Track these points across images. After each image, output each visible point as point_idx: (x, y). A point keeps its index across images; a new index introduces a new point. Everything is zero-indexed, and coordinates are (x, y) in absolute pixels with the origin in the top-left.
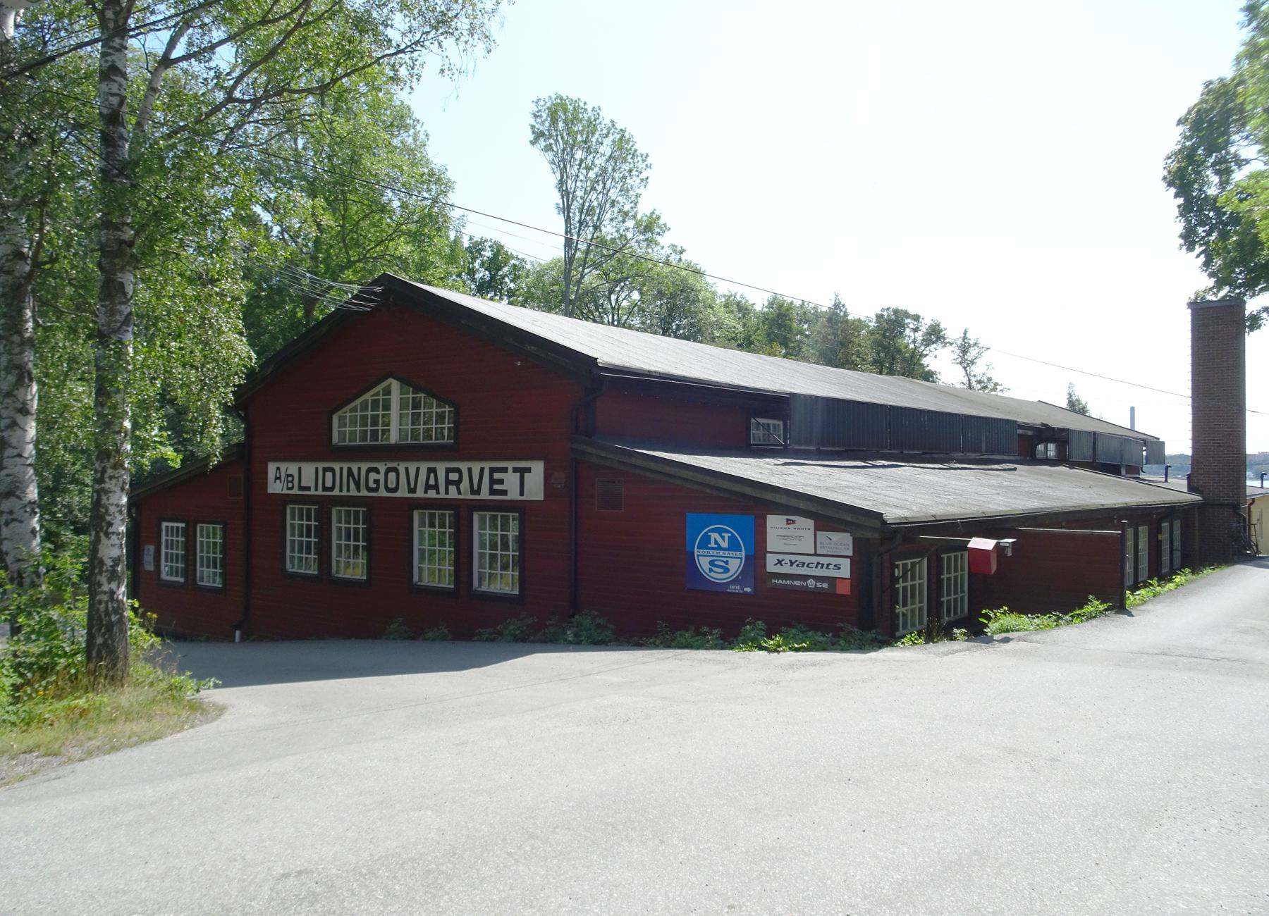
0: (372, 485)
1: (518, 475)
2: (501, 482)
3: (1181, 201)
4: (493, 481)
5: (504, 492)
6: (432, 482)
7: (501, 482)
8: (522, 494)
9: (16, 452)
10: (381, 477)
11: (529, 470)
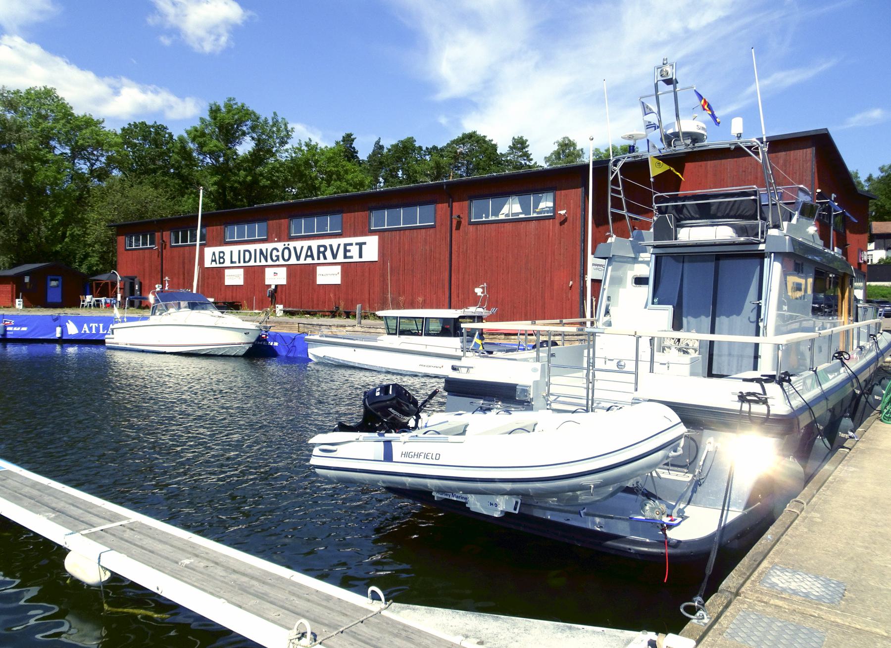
0: (275, 258)
1: (358, 247)
2: (349, 251)
3: (183, 304)
4: (346, 251)
5: (351, 257)
6: (309, 254)
7: (349, 251)
8: (361, 256)
9: (118, 85)
10: (280, 254)
11: (365, 243)
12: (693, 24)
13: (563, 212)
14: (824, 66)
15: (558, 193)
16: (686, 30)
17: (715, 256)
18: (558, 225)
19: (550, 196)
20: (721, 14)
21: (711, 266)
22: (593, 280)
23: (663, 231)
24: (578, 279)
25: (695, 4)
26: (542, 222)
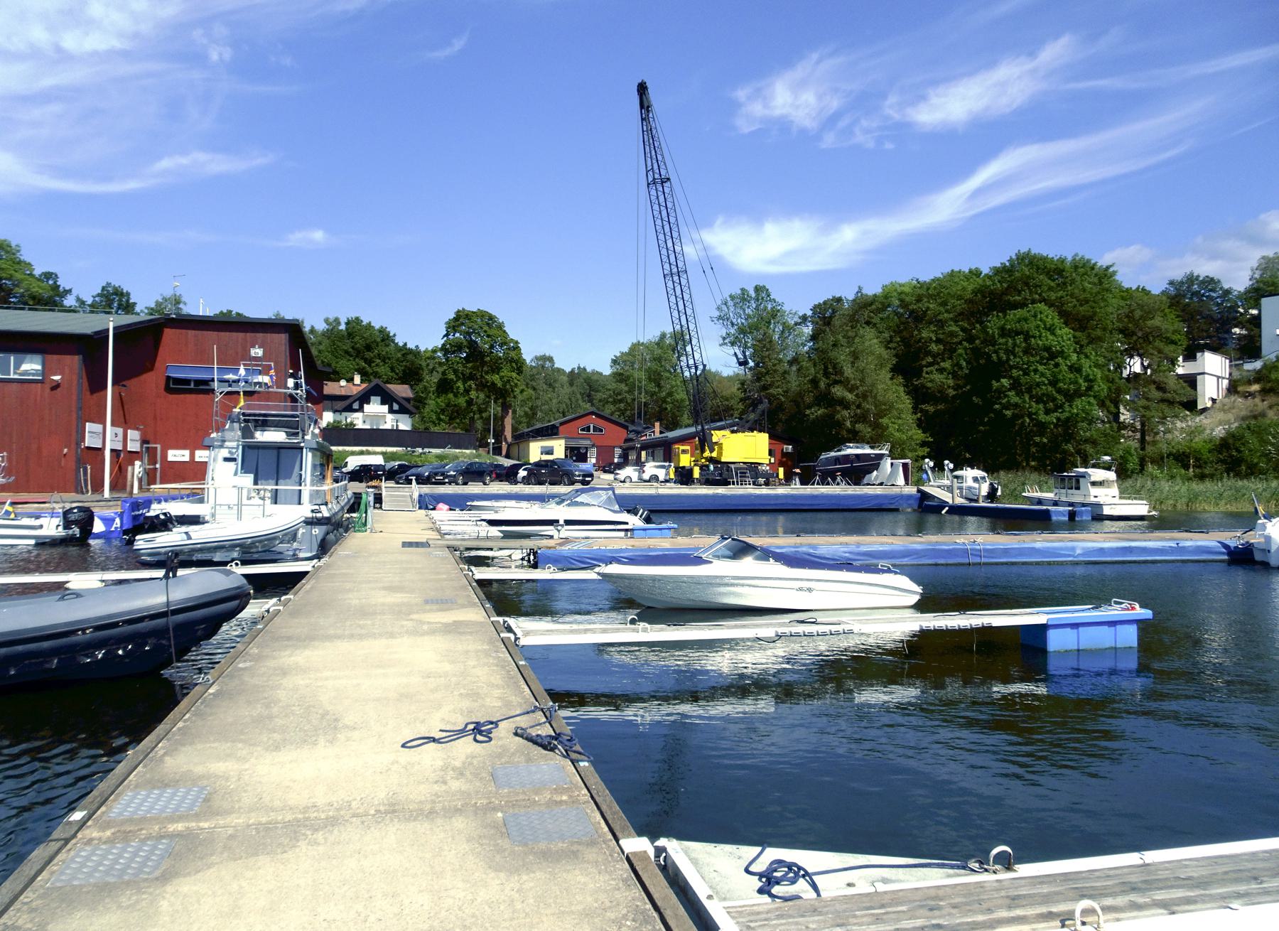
12: (71, 41)
13: (57, 378)
14: (260, 160)
15: (49, 356)
16: (59, 49)
17: (278, 448)
18: (48, 390)
19: (38, 358)
20: (116, 44)
21: (275, 452)
22: (112, 450)
23: (247, 433)
24: (73, 446)
25: (74, 16)
26: (26, 385)
